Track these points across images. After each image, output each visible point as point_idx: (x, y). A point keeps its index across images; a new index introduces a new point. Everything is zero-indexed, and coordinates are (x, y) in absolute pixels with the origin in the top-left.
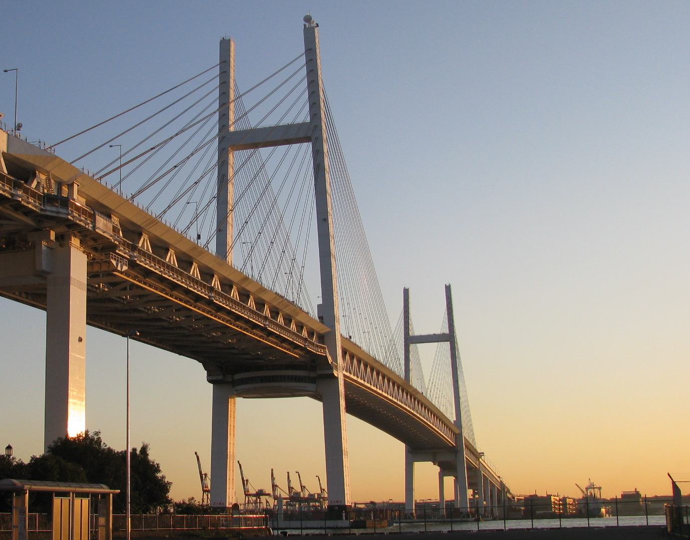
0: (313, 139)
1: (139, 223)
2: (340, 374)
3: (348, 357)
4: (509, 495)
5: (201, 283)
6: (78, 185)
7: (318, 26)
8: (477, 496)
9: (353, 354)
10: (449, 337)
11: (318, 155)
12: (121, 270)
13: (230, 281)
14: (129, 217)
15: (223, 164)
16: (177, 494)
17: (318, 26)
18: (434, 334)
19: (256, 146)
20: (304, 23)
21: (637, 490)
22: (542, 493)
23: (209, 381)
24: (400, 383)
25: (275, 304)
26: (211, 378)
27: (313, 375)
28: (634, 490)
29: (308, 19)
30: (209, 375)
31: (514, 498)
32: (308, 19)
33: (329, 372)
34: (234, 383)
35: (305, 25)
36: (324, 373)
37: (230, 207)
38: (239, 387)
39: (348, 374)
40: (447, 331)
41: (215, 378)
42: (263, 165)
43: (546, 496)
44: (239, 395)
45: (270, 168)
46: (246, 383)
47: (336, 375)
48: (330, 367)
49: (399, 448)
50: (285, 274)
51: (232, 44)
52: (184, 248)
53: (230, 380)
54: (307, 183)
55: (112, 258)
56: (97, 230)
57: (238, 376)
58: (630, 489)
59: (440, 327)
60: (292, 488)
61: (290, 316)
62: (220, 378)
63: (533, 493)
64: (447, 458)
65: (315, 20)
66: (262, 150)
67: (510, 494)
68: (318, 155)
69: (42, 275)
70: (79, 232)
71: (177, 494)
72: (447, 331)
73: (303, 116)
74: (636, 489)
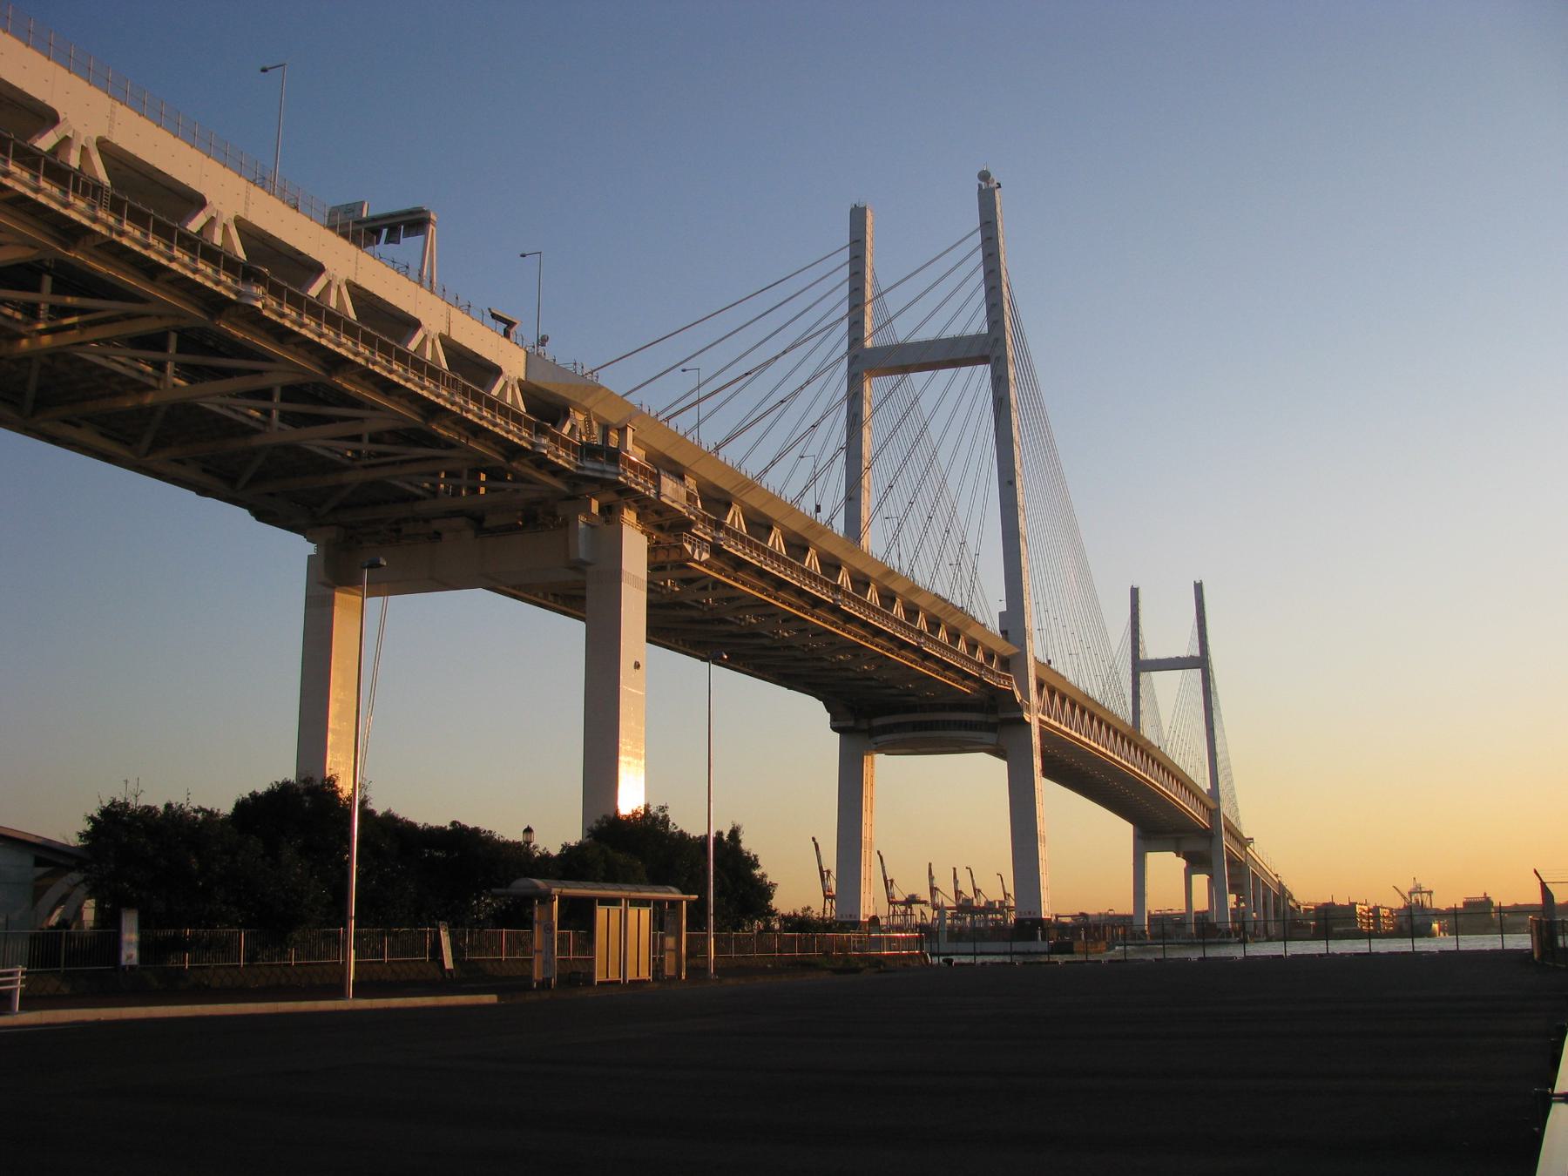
0: (993, 360)
1: (727, 488)
2: (1033, 718)
3: (1045, 692)
4: (1291, 903)
5: (821, 579)
6: (634, 430)
7: (1000, 187)
8: (1243, 905)
9: (1054, 689)
10: (1201, 662)
11: (1000, 384)
12: (700, 558)
13: (866, 576)
14: (712, 478)
15: (855, 398)
16: (785, 902)
17: (1000, 187)
18: (1178, 658)
19: (905, 369)
20: (979, 182)
21: (1488, 896)
22: (1341, 901)
23: (834, 729)
24: (1124, 732)
25: (934, 611)
26: (836, 725)
27: (992, 719)
28: (1483, 896)
29: (984, 176)
30: (833, 719)
31: (1299, 907)
32: (984, 176)
33: (1017, 715)
34: (872, 732)
35: (980, 186)
36: (1009, 716)
37: (865, 463)
38: (879, 739)
39: (1045, 718)
40: (1197, 653)
41: (842, 724)
42: (917, 399)
43: (1348, 904)
44: (881, 749)
45: (926, 404)
46: (891, 732)
47: (1027, 719)
48: (1018, 708)
49: (1122, 831)
50: (950, 565)
51: (869, 213)
52: (795, 526)
53: (866, 727)
54: (981, 435)
55: (686, 541)
56: (663, 499)
57: (877, 722)
58: (1477, 894)
59: (1188, 648)
60: (961, 892)
61: (957, 629)
62: (851, 723)
63: (1328, 900)
64: (1199, 846)
65: (996, 177)
66: (915, 376)
67: (1294, 901)
68: (1000, 384)
69: (579, 566)
70: (636, 502)
71: (785, 902)
72: (1197, 653)
73: (978, 324)
74: (1485, 894)
